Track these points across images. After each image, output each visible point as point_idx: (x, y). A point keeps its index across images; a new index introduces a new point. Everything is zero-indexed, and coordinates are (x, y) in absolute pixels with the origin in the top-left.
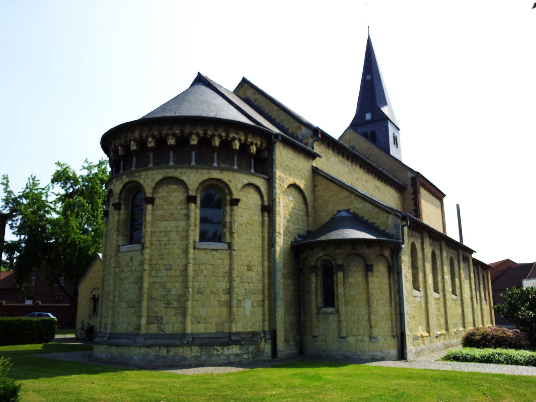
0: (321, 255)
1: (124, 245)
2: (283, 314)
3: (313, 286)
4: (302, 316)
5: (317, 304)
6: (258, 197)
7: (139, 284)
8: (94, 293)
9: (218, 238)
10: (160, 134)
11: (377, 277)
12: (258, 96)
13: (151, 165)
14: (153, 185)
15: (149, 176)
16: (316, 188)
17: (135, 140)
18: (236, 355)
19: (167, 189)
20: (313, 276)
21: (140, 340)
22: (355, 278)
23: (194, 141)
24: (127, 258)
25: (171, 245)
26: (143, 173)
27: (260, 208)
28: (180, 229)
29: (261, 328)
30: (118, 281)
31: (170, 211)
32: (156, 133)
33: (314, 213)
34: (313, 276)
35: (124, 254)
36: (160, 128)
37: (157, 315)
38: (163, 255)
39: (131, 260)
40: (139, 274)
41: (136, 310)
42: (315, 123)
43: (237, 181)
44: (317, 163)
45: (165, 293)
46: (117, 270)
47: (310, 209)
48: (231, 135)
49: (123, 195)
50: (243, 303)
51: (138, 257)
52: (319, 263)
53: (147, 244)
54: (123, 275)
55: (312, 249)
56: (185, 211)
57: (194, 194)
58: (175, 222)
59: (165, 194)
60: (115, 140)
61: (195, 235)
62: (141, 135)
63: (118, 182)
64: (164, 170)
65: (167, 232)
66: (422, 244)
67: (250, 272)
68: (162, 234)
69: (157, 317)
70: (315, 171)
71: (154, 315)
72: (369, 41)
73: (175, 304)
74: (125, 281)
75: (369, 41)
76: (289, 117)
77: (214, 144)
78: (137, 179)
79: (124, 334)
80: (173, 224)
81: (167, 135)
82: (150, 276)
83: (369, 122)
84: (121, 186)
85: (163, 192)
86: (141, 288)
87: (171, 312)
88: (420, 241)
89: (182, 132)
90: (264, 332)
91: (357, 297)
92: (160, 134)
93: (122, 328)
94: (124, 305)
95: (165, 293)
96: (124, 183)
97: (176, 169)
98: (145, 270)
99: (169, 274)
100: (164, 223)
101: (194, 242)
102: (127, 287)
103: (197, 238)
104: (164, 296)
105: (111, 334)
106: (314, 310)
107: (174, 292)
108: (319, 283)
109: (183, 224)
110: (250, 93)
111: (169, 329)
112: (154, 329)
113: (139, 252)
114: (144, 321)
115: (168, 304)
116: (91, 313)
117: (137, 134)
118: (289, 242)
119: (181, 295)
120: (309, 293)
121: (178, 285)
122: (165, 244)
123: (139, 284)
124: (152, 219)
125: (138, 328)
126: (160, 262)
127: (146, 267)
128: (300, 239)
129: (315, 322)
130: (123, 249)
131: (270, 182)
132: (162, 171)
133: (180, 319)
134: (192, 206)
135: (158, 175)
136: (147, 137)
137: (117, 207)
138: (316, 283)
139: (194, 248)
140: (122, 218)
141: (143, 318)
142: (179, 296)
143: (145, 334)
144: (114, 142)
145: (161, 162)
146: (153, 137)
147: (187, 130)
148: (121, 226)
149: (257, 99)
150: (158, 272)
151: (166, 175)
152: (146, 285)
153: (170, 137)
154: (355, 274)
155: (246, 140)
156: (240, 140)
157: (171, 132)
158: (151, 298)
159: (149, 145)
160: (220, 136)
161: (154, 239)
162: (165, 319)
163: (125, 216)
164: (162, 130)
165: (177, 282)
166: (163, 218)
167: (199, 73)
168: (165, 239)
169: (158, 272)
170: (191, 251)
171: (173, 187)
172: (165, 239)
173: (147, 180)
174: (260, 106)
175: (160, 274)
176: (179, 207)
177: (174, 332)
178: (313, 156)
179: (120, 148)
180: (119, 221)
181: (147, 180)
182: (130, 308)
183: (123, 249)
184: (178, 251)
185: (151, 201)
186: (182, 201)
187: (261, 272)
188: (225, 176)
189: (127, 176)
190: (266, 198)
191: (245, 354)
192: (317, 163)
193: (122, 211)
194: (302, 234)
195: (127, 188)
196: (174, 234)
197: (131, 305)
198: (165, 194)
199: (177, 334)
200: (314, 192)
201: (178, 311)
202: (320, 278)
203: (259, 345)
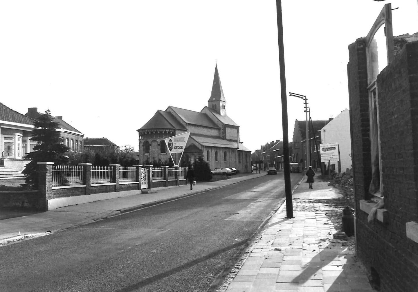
42: (196, 111)
66: (212, 151)
72: (216, 66)
75: (216, 66)
88: (211, 151)
89: (156, 131)
103: (160, 152)
134: (159, 146)
167: (137, 131)
170: (159, 155)
185: (151, 145)
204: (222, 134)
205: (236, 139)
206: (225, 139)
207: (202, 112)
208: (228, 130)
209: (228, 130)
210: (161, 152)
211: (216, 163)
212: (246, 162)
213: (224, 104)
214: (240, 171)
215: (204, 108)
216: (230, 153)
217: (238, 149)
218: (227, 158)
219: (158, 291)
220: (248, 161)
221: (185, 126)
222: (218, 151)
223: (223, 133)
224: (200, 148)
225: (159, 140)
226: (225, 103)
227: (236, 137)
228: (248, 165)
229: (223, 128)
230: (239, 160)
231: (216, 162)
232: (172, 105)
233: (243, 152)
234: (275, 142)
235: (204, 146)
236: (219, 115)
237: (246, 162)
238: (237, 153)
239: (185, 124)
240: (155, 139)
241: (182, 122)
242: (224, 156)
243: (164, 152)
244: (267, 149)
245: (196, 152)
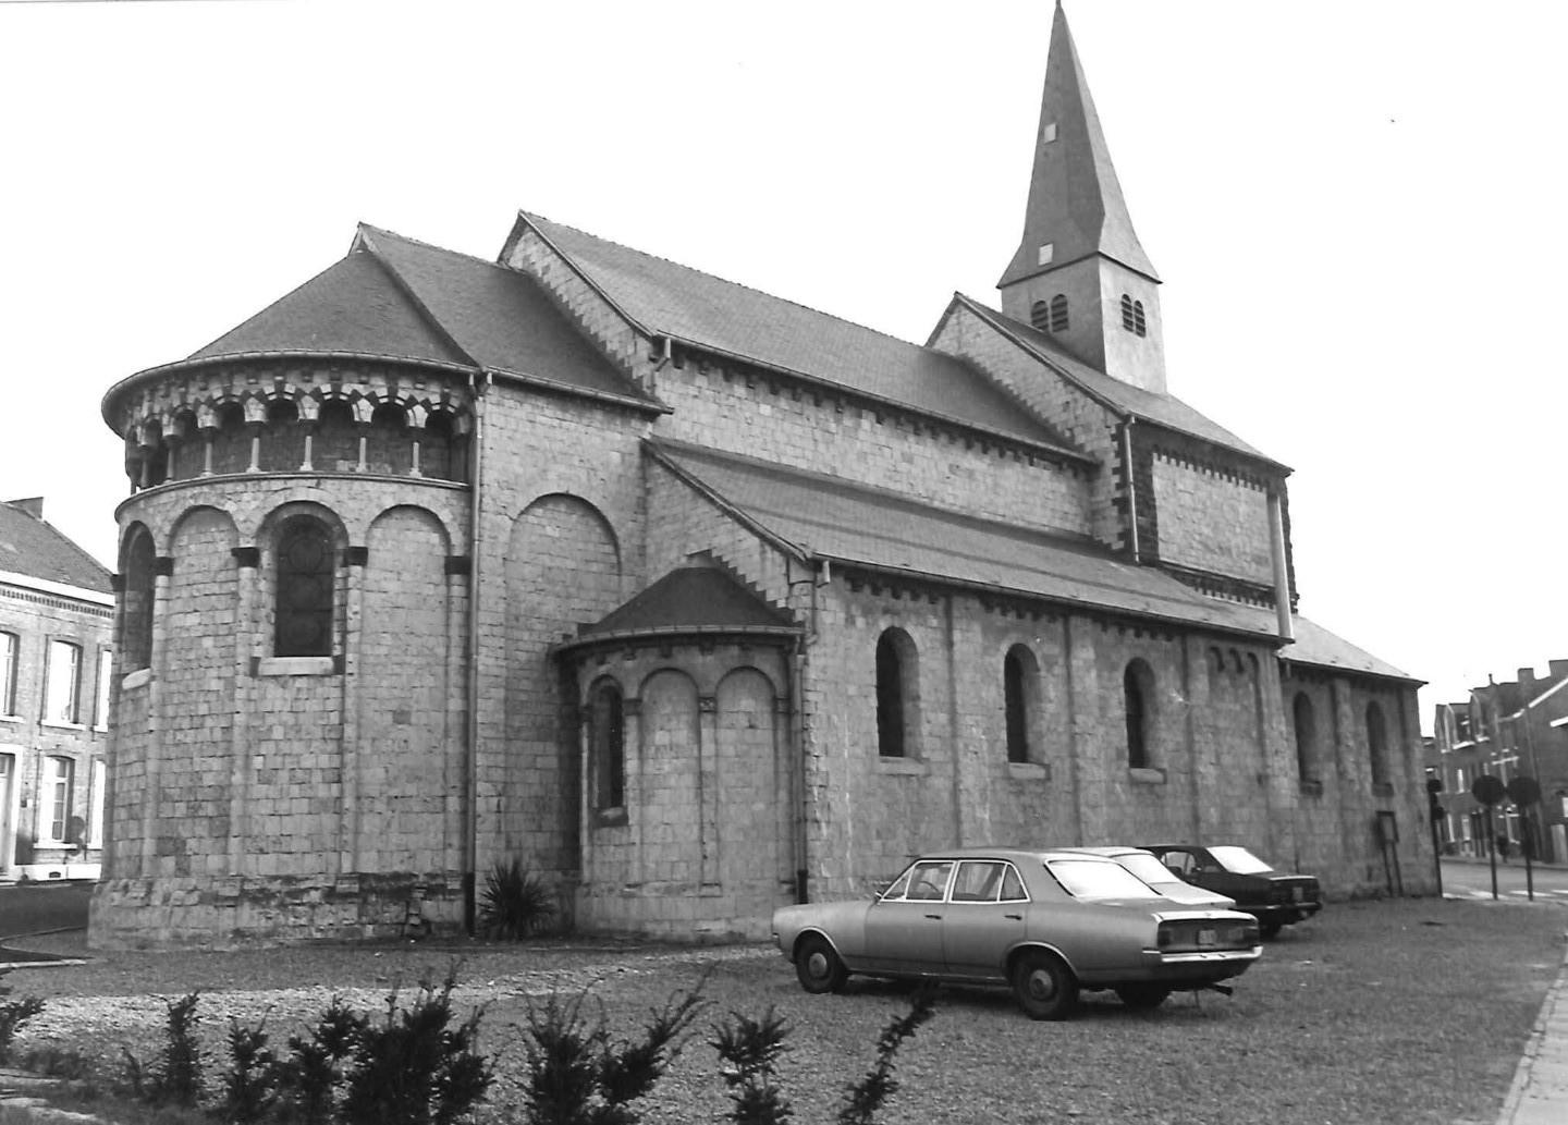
6: (435, 538)
9: (317, 645)
11: (731, 727)
22: (669, 731)
23: (310, 411)
27: (442, 562)
43: (355, 498)
48: (347, 389)
72: (1059, 12)
75: (1059, 12)
81: (299, 394)
83: (1050, 269)
87: (201, 828)
91: (672, 781)
98: (634, 844)
153: (203, 408)
154: (669, 720)
155: (392, 395)
156: (372, 398)
157: (308, 388)
160: (317, 394)
164: (232, 386)
185: (166, 566)
188: (328, 494)
190: (457, 538)
204: (1114, 512)
205: (1262, 575)
206: (1151, 561)
207: (938, 346)
208: (1171, 481)
209: (1171, 481)
210: (282, 647)
211: (1019, 788)
212: (1383, 787)
213: (1135, 296)
214: (1323, 885)
215: (949, 312)
216: (1201, 684)
217: (1288, 652)
218: (1166, 739)
219: (1126, 1119)
220: (1396, 774)
221: (642, 371)
222: (1044, 647)
223: (1122, 504)
224: (776, 594)
225: (249, 505)
226: (1146, 284)
227: (1259, 560)
228: (1401, 817)
229: (1121, 453)
230: (1303, 759)
231: (1023, 771)
232: (559, 210)
233: (1344, 689)
234: (1542, 672)
235: (815, 564)
236: (1098, 375)
237: (1383, 787)
238: (1274, 693)
239: (644, 348)
240: (206, 496)
241: (613, 337)
242: (1118, 712)
243: (319, 647)
244: (1485, 720)
245: (706, 642)
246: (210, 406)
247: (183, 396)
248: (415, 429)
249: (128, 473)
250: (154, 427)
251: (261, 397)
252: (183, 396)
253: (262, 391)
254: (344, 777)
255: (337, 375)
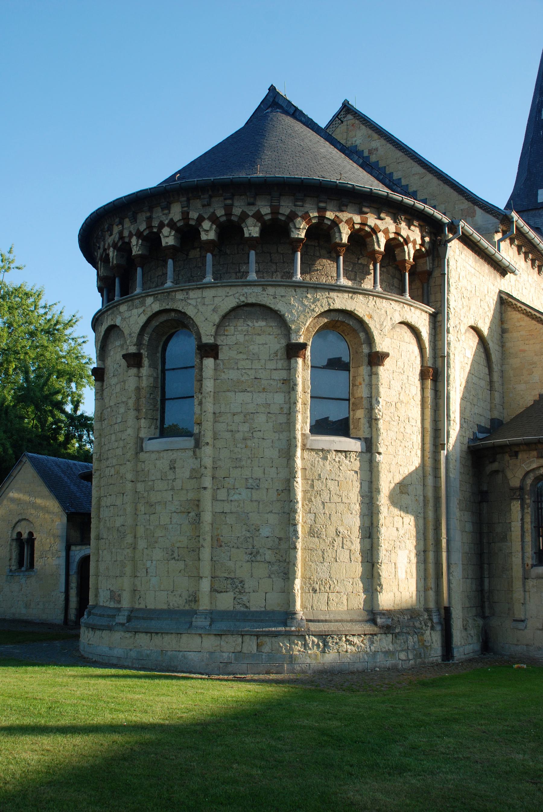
0: (534, 466)
1: (150, 439)
2: (461, 577)
3: (516, 526)
4: (486, 581)
5: (523, 559)
7: (192, 514)
8: (19, 529)
9: (342, 428)
10: (229, 214)
12: (378, 143)
13: (209, 279)
14: (216, 319)
15: (207, 301)
16: (506, 335)
17: (172, 225)
18: (387, 653)
19: (245, 328)
20: (516, 506)
21: (200, 622)
24: (163, 464)
25: (256, 440)
26: (192, 294)
28: (275, 409)
29: (422, 603)
30: (142, 508)
31: (252, 373)
32: (220, 212)
33: (503, 384)
34: (516, 506)
35: (154, 456)
36: (229, 202)
37: (232, 576)
38: (241, 460)
39: (173, 468)
40: (191, 495)
41: (186, 565)
44: (508, 284)
45: (248, 535)
46: (140, 487)
47: (496, 377)
49: (146, 338)
50: (393, 555)
51: (186, 464)
52: (529, 482)
53: (208, 437)
54: (154, 497)
55: (516, 455)
56: (283, 374)
57: (211, 341)
58: (263, 395)
59: (240, 338)
60: (121, 223)
61: (303, 423)
62: (185, 216)
63: (135, 311)
64: (239, 289)
65: (248, 414)
67: (405, 496)
68: (238, 419)
69: (232, 579)
70: (505, 302)
71: (226, 575)
73: (269, 555)
74: (158, 508)
76: (448, 189)
77: (338, 241)
78: (179, 306)
79: (162, 611)
80: (260, 398)
81: (244, 216)
82: (215, 499)
84: (143, 319)
85: (236, 335)
86: (197, 521)
87: (261, 571)
89: (275, 212)
90: (427, 610)
92: (229, 214)
93: (155, 599)
94: (158, 554)
95: (248, 535)
96: (149, 314)
97: (264, 286)
98: (205, 488)
99: (254, 498)
100: (241, 397)
101: (303, 435)
102: (165, 520)
104: (246, 539)
105: (132, 610)
106: (517, 571)
107: (265, 531)
108: (528, 519)
109: (279, 398)
110: (359, 137)
111: (256, 603)
112: (226, 602)
113: (191, 453)
114: (205, 585)
115: (254, 555)
116: (14, 568)
117: (176, 213)
118: (466, 441)
119: (280, 539)
120: (505, 538)
121: (273, 519)
122: (245, 439)
123: (192, 514)
124: (215, 387)
125: (194, 599)
126: (235, 473)
127: (207, 482)
128: (481, 436)
129: (518, 594)
130: (149, 445)
131: (437, 321)
132: (234, 290)
133: (279, 583)
135: (226, 298)
136: (201, 219)
137: (133, 360)
138: (522, 519)
139: (304, 448)
140: (145, 383)
141: (204, 580)
142: (277, 540)
143: (211, 612)
144: (116, 229)
145: (229, 272)
146: (213, 219)
147: (285, 209)
148: (143, 400)
149: (377, 149)
150: (232, 492)
151: (243, 299)
152: (207, 517)
153: (250, 221)
158: (218, 543)
159: (204, 237)
161: (221, 427)
162: (249, 584)
163: (151, 380)
164: (232, 205)
165: (271, 512)
166: (238, 387)
167: (272, 89)
168: (245, 428)
169: (232, 492)
171: (256, 325)
172: (245, 428)
173: (202, 309)
174: (381, 164)
175: (236, 497)
176: (271, 365)
177: (268, 608)
178: (502, 270)
179: (134, 241)
180: (138, 389)
181: (202, 309)
182: (173, 561)
183: (151, 445)
184: (271, 453)
186: (276, 353)
187: (422, 498)
189: (156, 299)
191: (402, 650)
192: (508, 284)
193: (145, 371)
194: (483, 425)
195: (155, 323)
196: (262, 418)
197: (176, 555)
198: (240, 338)
199: (273, 612)
200: (502, 345)
201: (275, 568)
202: (529, 510)
203: (423, 634)
240: (254, 295)
246: (213, 222)
247: (149, 219)
248: (252, 238)
249: (100, 290)
250: (124, 248)
251: (258, 216)
252: (149, 219)
253: (258, 212)
254: (197, 499)
255: (252, 200)
